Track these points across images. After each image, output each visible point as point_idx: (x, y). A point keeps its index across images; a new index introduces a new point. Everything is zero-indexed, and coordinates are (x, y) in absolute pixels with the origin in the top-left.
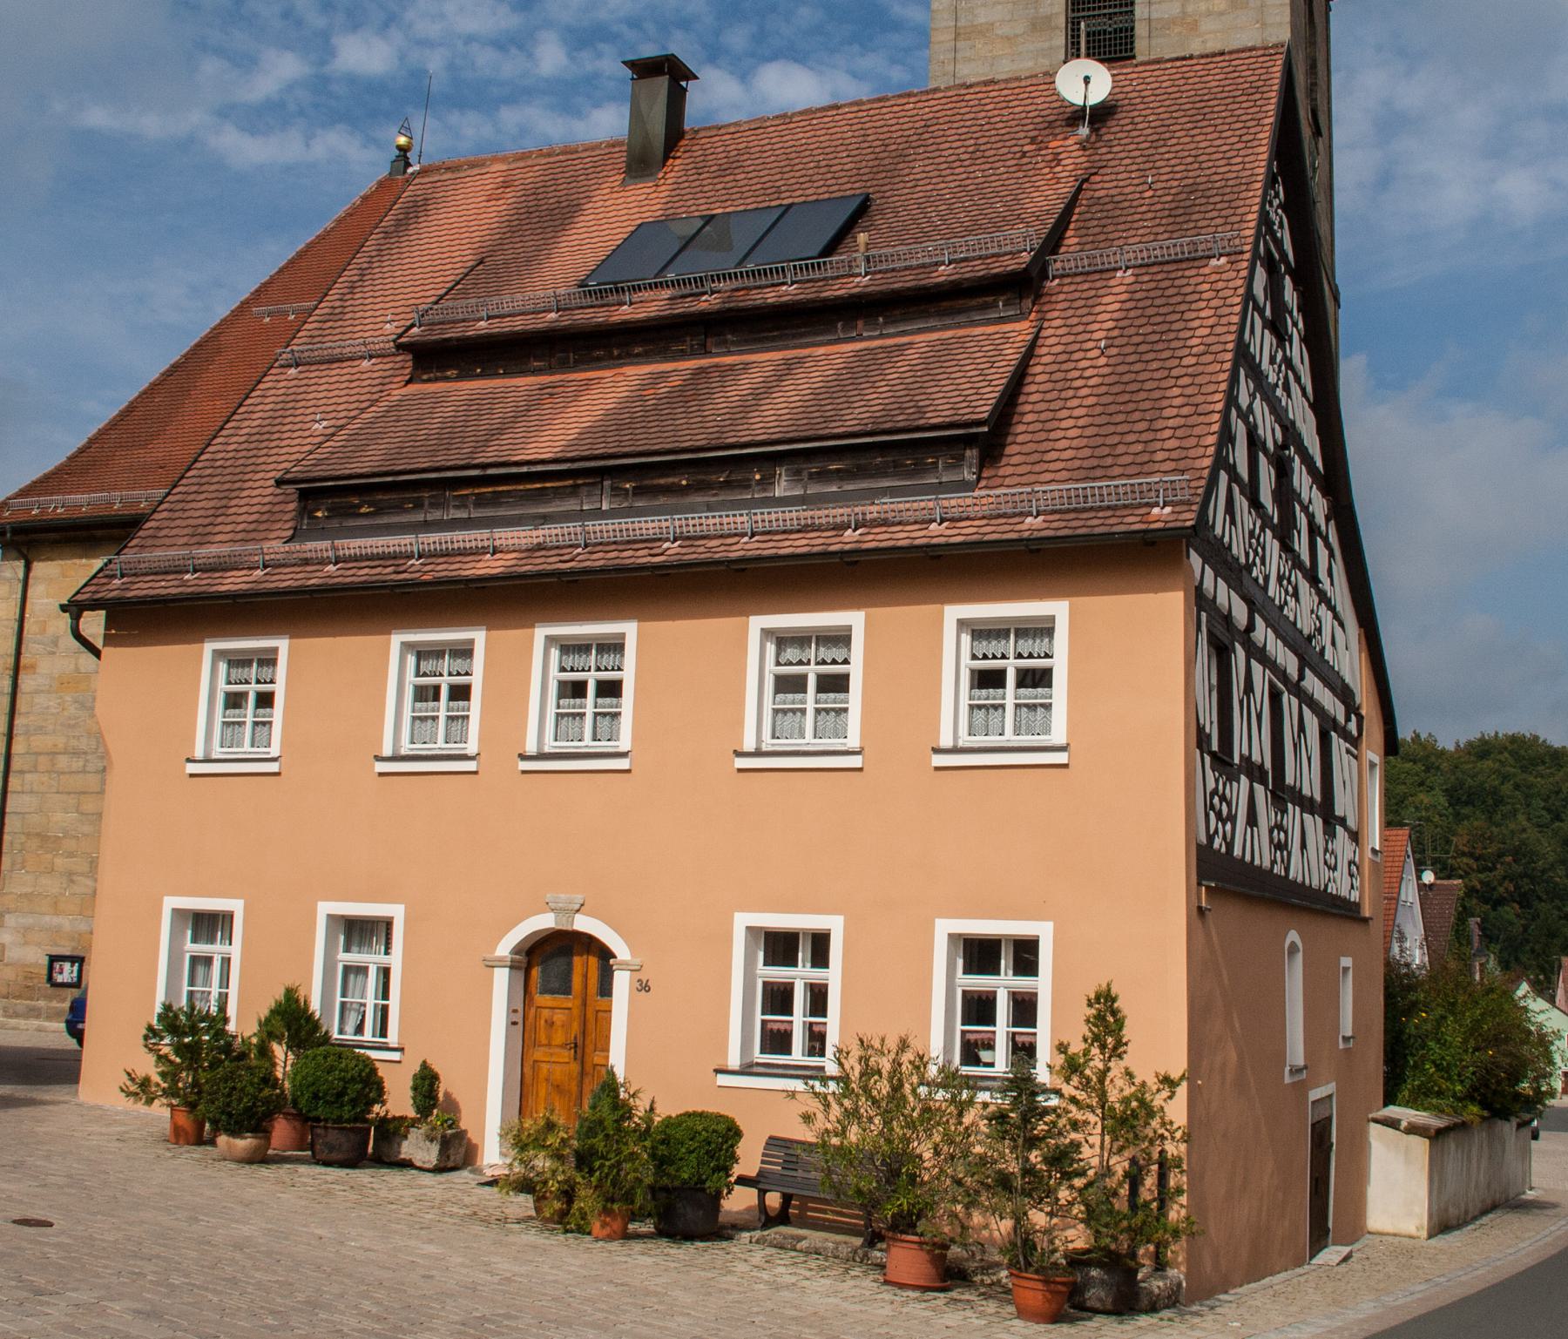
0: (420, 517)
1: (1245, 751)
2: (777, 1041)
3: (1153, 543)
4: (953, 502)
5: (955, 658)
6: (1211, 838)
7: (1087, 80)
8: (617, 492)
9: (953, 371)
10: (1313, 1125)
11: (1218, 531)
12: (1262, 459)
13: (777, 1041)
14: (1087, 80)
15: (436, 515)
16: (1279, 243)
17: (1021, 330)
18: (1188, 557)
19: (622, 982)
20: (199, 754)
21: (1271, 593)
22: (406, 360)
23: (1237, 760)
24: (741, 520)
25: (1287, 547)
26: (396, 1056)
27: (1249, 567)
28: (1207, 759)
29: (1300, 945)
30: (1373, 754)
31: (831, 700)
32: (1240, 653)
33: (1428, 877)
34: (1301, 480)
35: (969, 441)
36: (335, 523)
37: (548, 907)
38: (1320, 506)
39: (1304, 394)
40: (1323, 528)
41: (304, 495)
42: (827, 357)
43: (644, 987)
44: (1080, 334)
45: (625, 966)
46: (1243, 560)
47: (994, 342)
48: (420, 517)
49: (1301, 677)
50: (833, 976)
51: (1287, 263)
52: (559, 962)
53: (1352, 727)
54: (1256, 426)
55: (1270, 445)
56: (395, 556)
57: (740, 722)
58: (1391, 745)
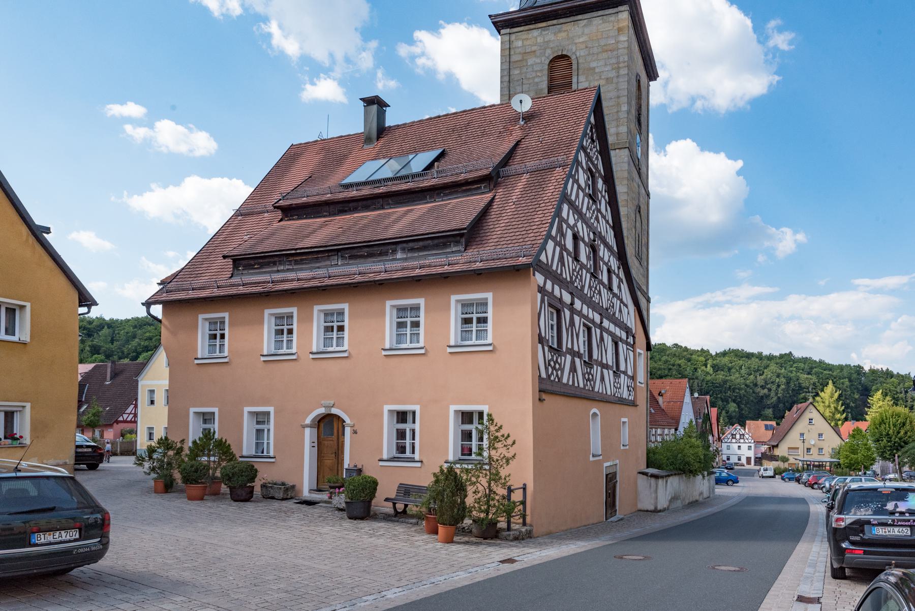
0: (275, 269)
1: (570, 346)
2: (401, 449)
3: (518, 270)
4: (453, 258)
5: (454, 316)
6: (549, 376)
7: (521, 102)
8: (343, 257)
9: (459, 211)
10: (607, 475)
11: (554, 268)
12: (582, 245)
13: (401, 449)
14: (521, 102)
15: (282, 268)
16: (596, 166)
17: (489, 196)
18: (534, 275)
19: (348, 431)
20: (199, 356)
21: (586, 292)
22: (279, 214)
23: (564, 350)
24: (380, 267)
25: (594, 276)
26: (419, 465)
27: (572, 282)
28: (546, 349)
29: (598, 413)
30: (641, 350)
31: (415, 331)
32: (567, 313)
33: (696, 395)
34: (603, 252)
35: (462, 235)
36: (246, 272)
37: (322, 406)
38: (614, 263)
39: (607, 222)
40: (616, 271)
41: (234, 261)
42: (421, 208)
43: (355, 432)
44: (509, 199)
45: (349, 425)
46: (569, 279)
47: (476, 202)
48: (275, 269)
49: (601, 323)
50: (417, 427)
51: (599, 172)
52: (328, 425)
53: (631, 340)
54: (578, 232)
55: (586, 239)
56: (264, 282)
57: (384, 339)
58: (649, 347)
